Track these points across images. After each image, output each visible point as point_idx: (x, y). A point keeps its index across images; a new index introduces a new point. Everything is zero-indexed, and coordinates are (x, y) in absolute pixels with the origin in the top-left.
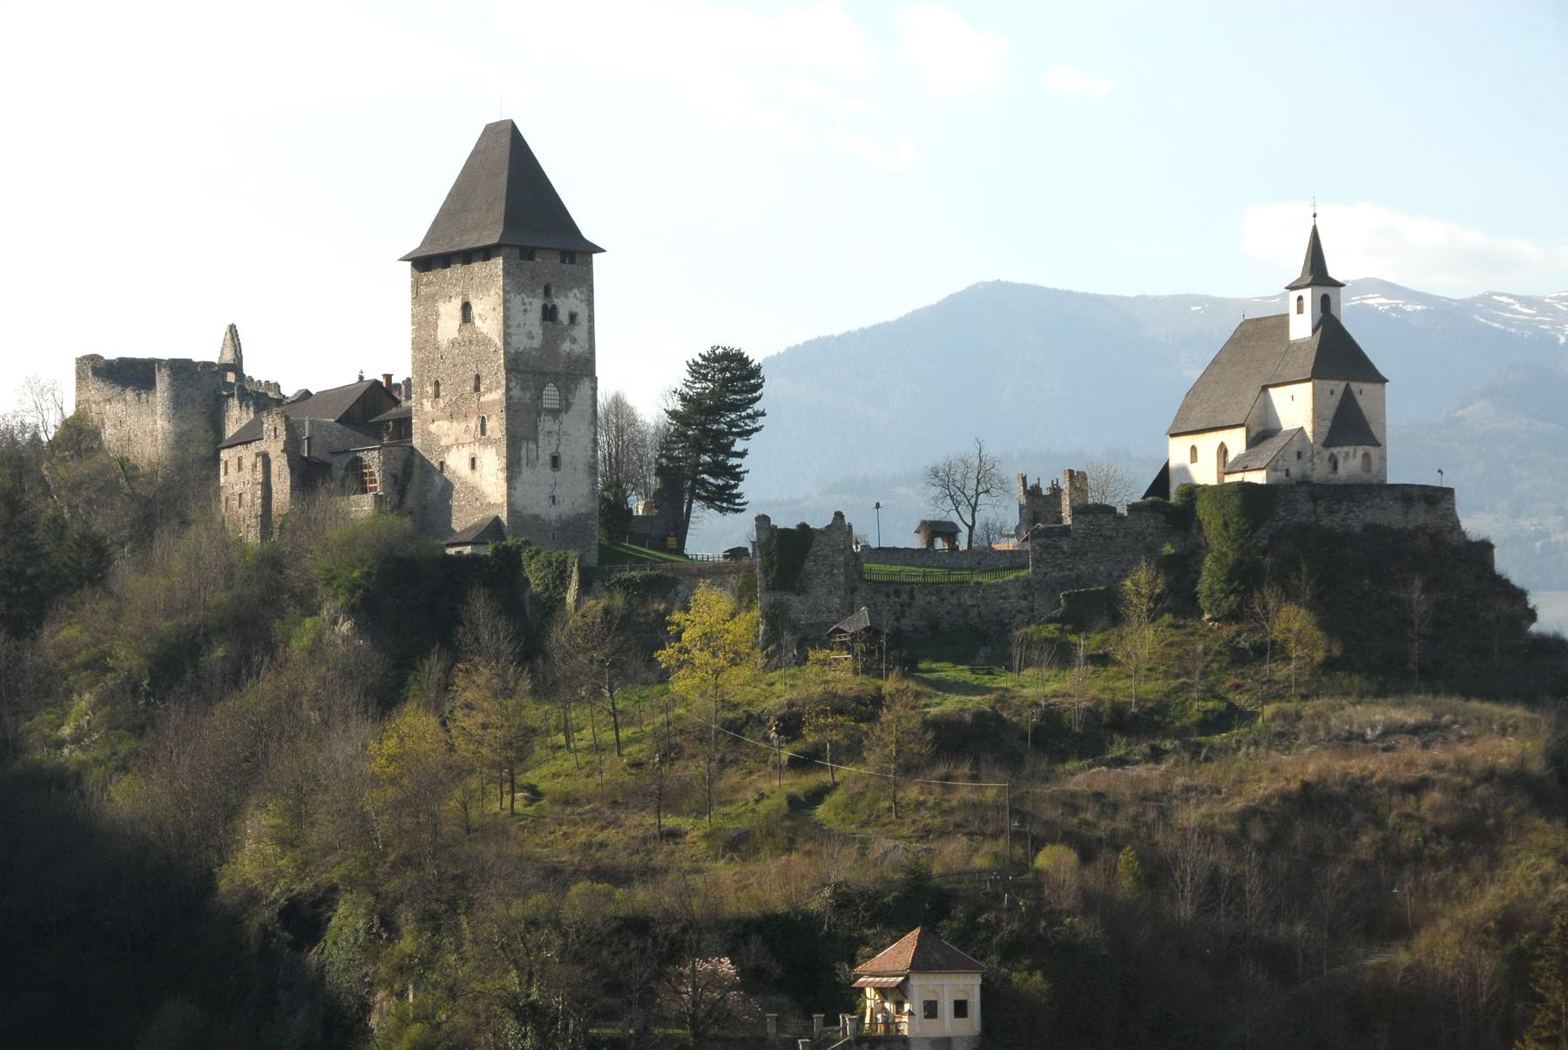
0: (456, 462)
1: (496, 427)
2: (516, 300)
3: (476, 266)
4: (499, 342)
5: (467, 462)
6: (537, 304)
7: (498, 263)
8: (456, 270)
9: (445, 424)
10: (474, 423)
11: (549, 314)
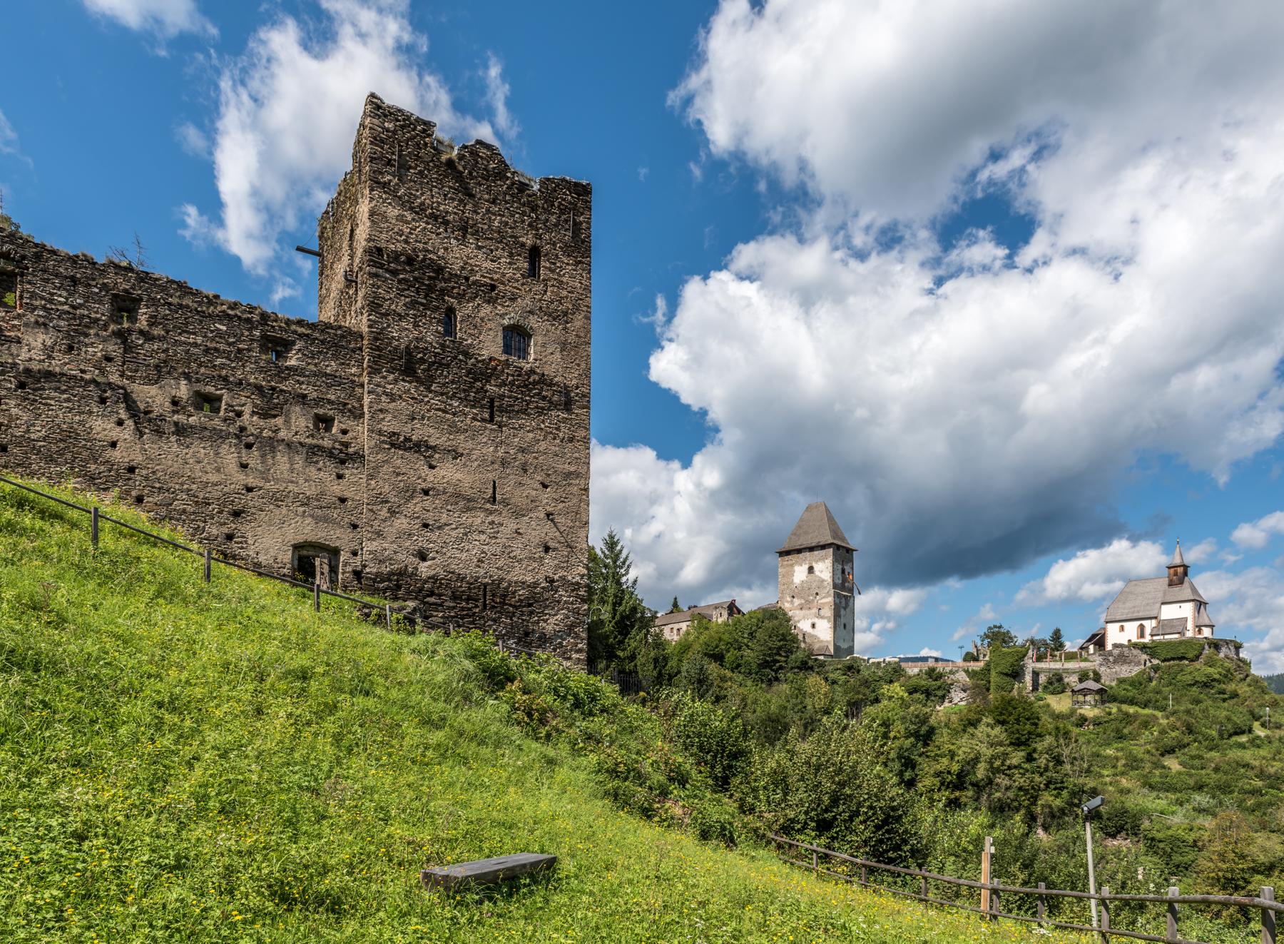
0: (804, 626)
1: (828, 612)
3: (816, 553)
4: (830, 580)
5: (810, 625)
6: (840, 567)
8: (808, 554)
10: (815, 610)
11: (843, 571)
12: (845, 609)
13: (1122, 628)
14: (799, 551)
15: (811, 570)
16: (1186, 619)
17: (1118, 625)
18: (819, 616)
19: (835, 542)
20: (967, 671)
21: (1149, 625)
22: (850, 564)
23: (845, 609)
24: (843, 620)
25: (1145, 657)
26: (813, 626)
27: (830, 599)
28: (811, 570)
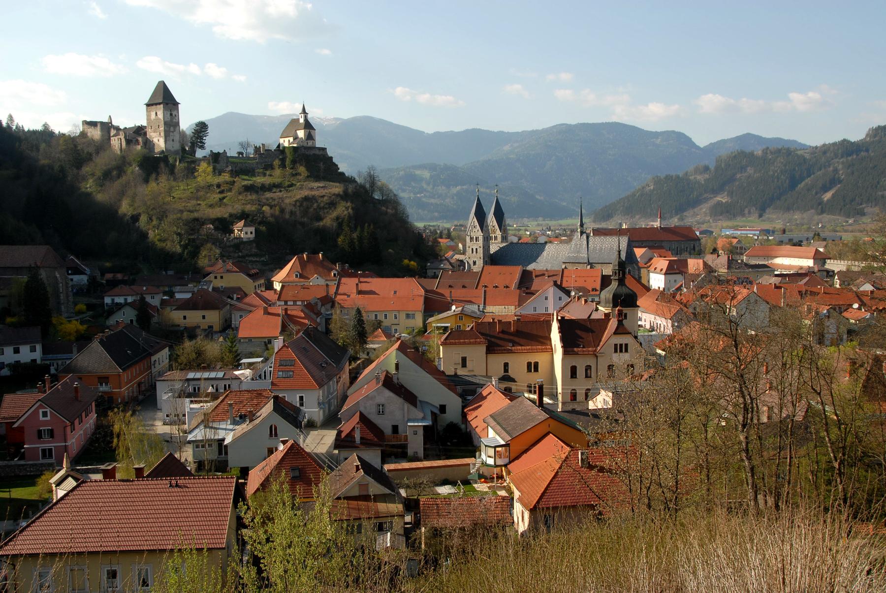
1: (162, 134)
2: (165, 112)
3: (158, 106)
6: (169, 113)
7: (162, 105)
10: (158, 133)
11: (171, 115)
15: (156, 113)
16: (14, 348)
23: (173, 132)
24: (171, 138)
27: (163, 128)
28: (156, 113)
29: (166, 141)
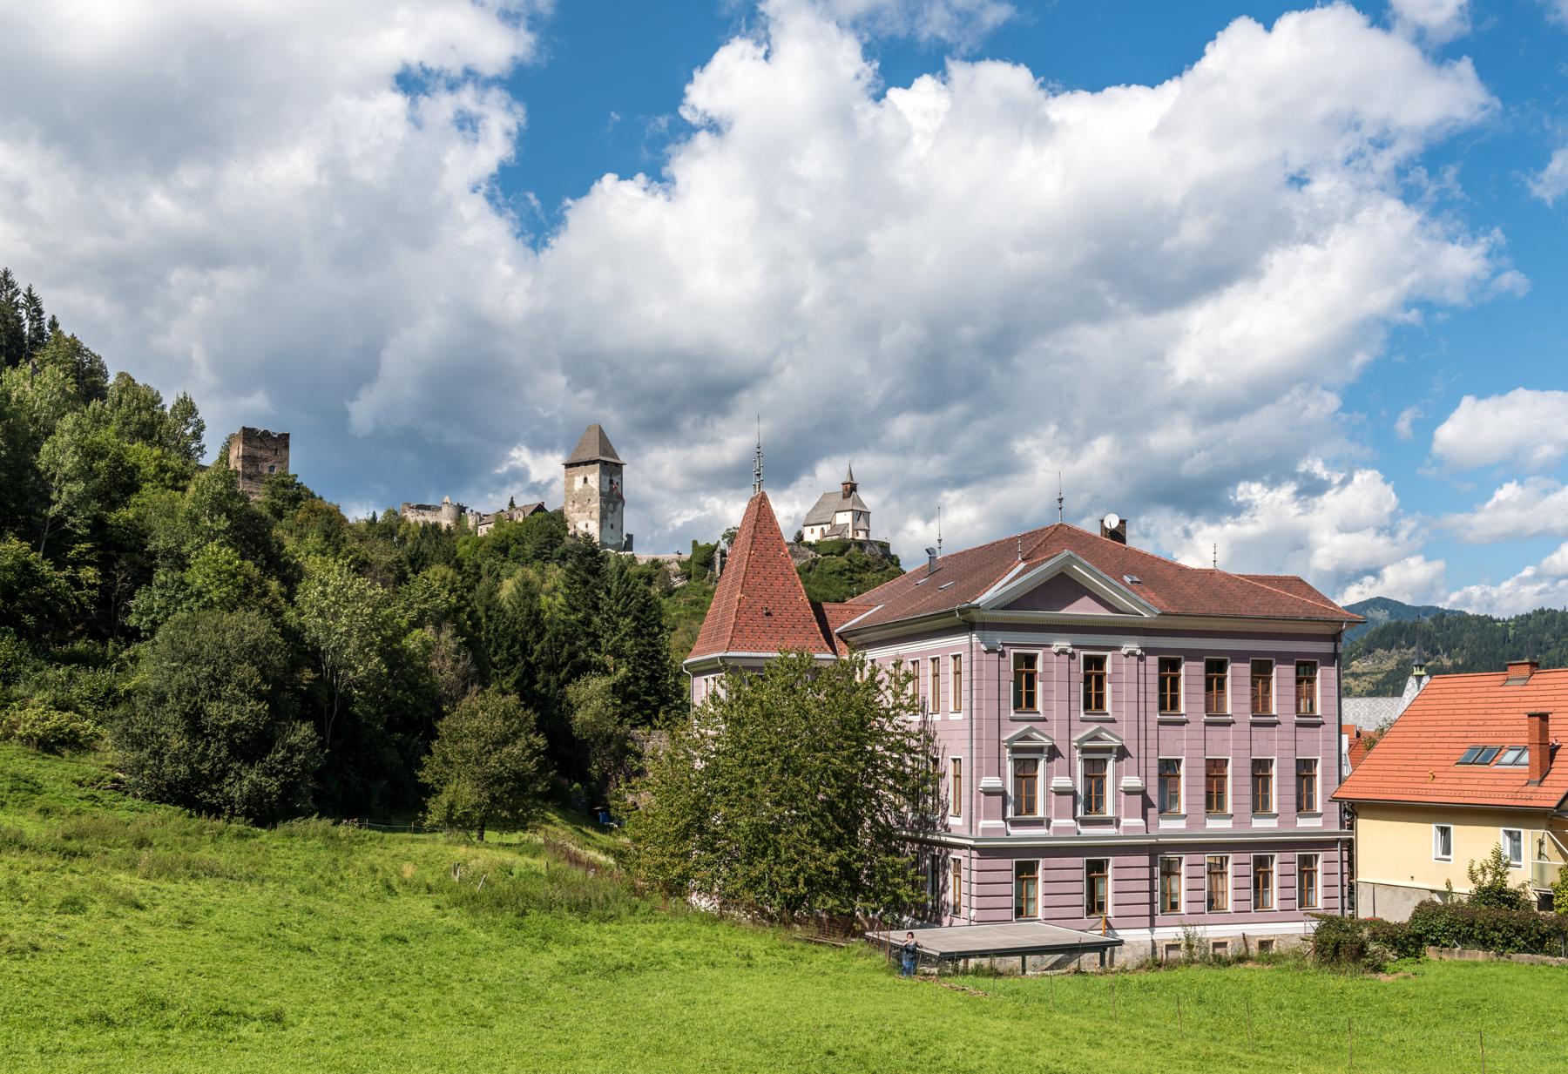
1: (596, 515)
2: (603, 477)
4: (598, 489)
8: (583, 467)
9: (577, 514)
11: (611, 482)
12: (612, 512)
13: (812, 531)
14: (578, 464)
15: (585, 480)
17: (810, 528)
18: (590, 518)
19: (602, 458)
20: (678, 562)
21: (827, 528)
22: (619, 476)
23: (612, 512)
24: (610, 522)
25: (811, 552)
26: (587, 526)
27: (598, 505)
28: (585, 480)
29: (601, 528)
